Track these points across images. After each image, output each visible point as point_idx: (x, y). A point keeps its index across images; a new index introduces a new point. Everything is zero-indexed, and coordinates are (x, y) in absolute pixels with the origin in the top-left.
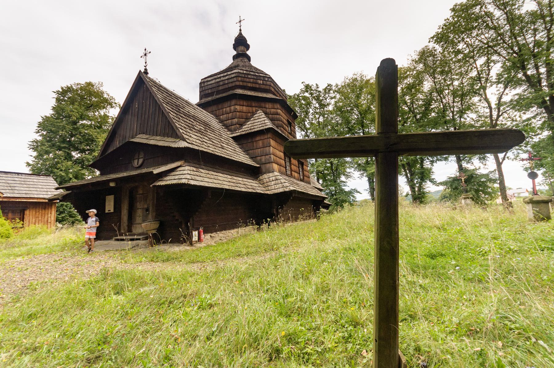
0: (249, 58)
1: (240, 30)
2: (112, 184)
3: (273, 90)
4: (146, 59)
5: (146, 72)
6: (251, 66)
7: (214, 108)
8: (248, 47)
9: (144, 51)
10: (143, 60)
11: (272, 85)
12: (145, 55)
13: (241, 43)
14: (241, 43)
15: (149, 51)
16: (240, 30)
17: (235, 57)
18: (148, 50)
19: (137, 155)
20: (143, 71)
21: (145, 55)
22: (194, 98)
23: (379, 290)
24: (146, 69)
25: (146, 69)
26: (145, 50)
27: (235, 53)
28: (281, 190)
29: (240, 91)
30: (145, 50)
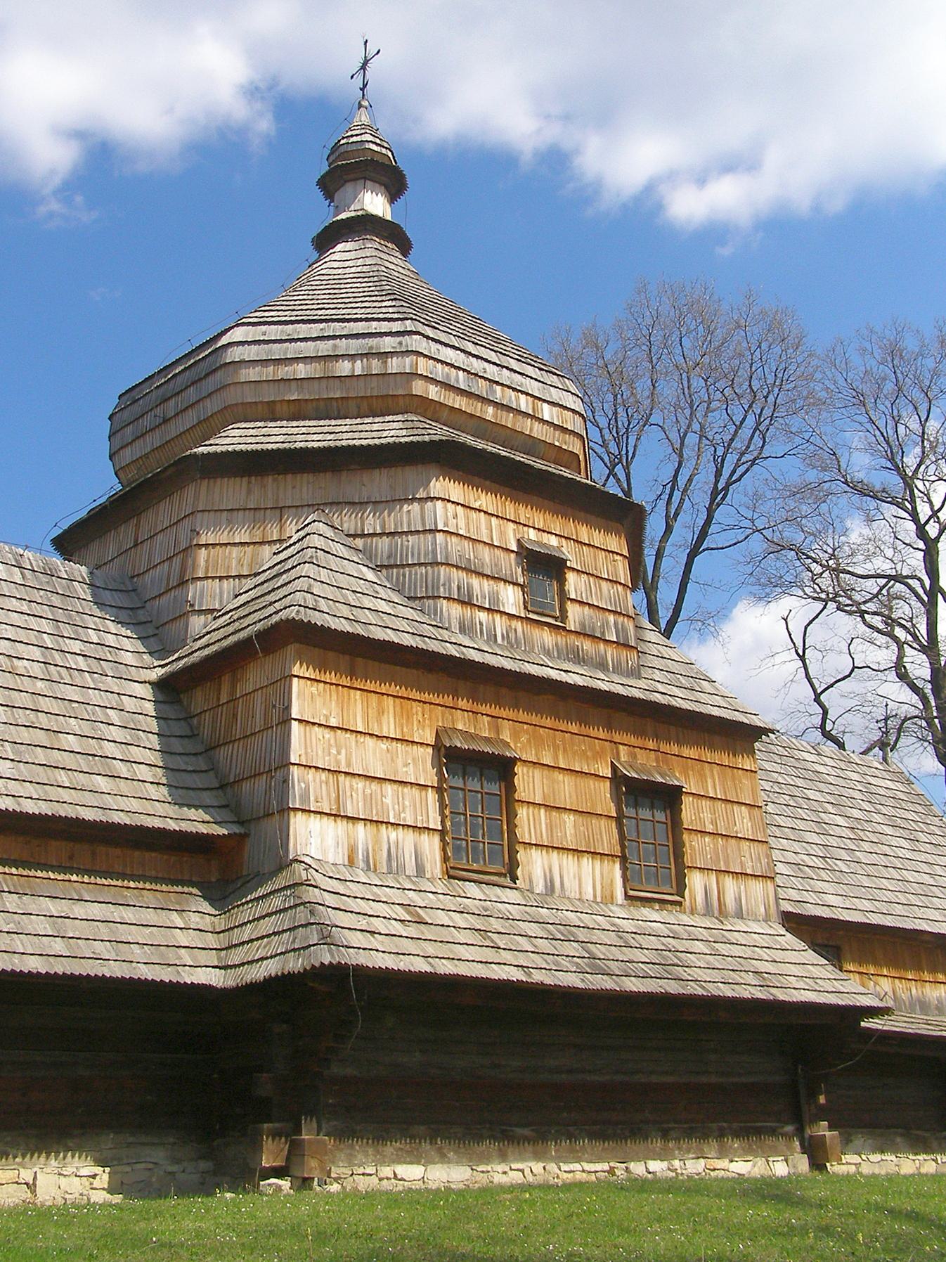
3: (433, 392)
11: (423, 366)
29: (238, 438)
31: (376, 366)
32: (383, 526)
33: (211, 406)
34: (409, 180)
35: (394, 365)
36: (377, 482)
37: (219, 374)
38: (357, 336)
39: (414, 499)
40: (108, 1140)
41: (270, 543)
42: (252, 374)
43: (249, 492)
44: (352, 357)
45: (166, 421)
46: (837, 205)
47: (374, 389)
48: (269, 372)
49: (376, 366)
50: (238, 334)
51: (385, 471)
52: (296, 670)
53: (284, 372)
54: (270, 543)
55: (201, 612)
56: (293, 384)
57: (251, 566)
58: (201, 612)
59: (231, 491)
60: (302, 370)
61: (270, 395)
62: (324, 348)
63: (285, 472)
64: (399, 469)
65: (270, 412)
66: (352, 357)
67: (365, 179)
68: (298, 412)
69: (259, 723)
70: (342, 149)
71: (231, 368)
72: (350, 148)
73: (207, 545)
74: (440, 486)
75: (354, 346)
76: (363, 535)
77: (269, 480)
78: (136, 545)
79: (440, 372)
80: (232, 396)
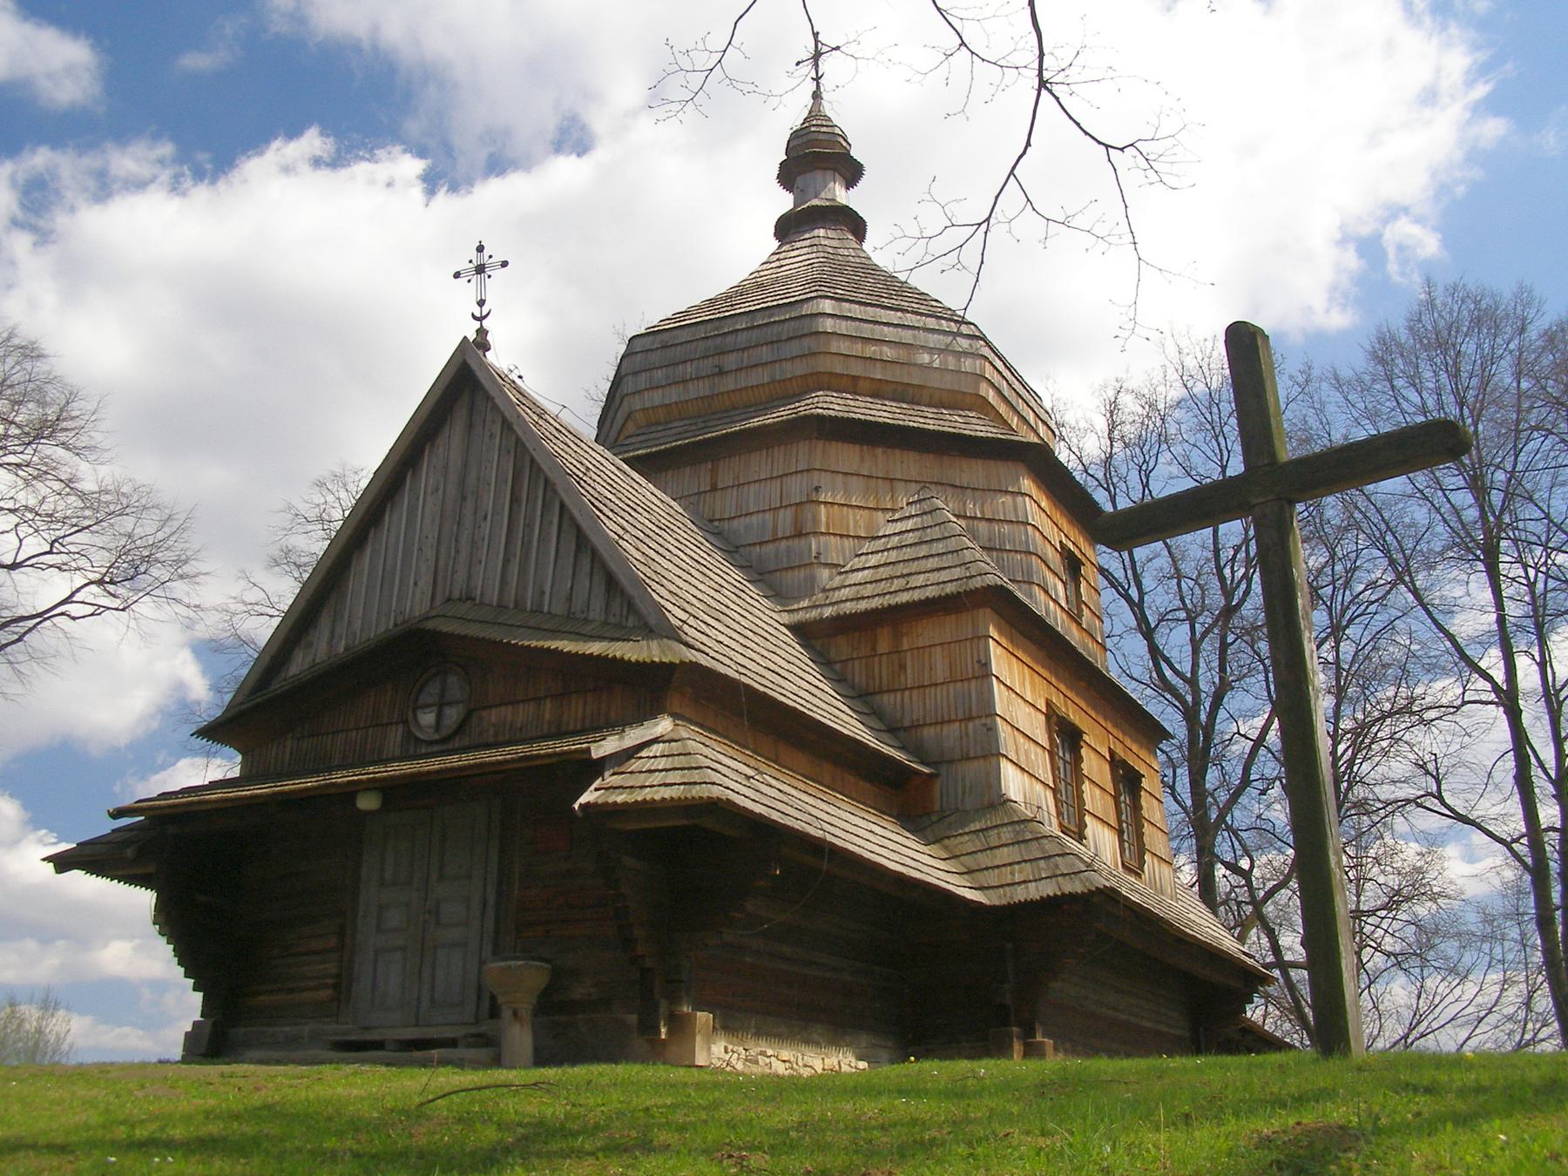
0: (857, 226)
1: (817, 96)
2: (368, 802)
3: (991, 396)
4: (482, 287)
5: (481, 342)
6: (871, 269)
7: (695, 478)
8: (852, 173)
9: (473, 255)
10: (467, 292)
11: (989, 372)
12: (480, 269)
13: (816, 156)
14: (816, 156)
15: (498, 258)
16: (817, 96)
17: (787, 229)
18: (495, 251)
19: (434, 689)
20: (472, 336)
21: (480, 269)
22: (590, 433)
23: (1260, 372)
24: (482, 332)
25: (482, 332)
26: (480, 249)
27: (784, 202)
28: (1048, 889)
29: (832, 404)
30: (480, 249)
31: (951, 363)
32: (982, 512)
33: (800, 368)
34: (861, 184)
35: (968, 365)
36: (973, 472)
37: (806, 342)
38: (933, 331)
39: (1007, 492)
40: (864, 1039)
41: (885, 510)
42: (844, 347)
43: (862, 459)
44: (931, 350)
45: (721, 373)
46: (379, 153)
47: (948, 383)
48: (858, 349)
49: (951, 363)
50: (827, 306)
51: (980, 462)
52: (993, 632)
53: (871, 350)
54: (885, 510)
55: (826, 565)
56: (878, 365)
57: (867, 528)
58: (826, 565)
59: (846, 456)
60: (888, 353)
61: (856, 369)
62: (907, 336)
63: (893, 446)
64: (897, 452)
65: (851, 385)
66: (931, 350)
67: (835, 170)
68: (879, 391)
69: (940, 673)
70: (813, 136)
71: (822, 337)
72: (821, 137)
73: (825, 503)
74: (1027, 484)
75: (933, 340)
76: (965, 517)
77: (879, 451)
78: (714, 489)
79: (996, 379)
80: (824, 364)
